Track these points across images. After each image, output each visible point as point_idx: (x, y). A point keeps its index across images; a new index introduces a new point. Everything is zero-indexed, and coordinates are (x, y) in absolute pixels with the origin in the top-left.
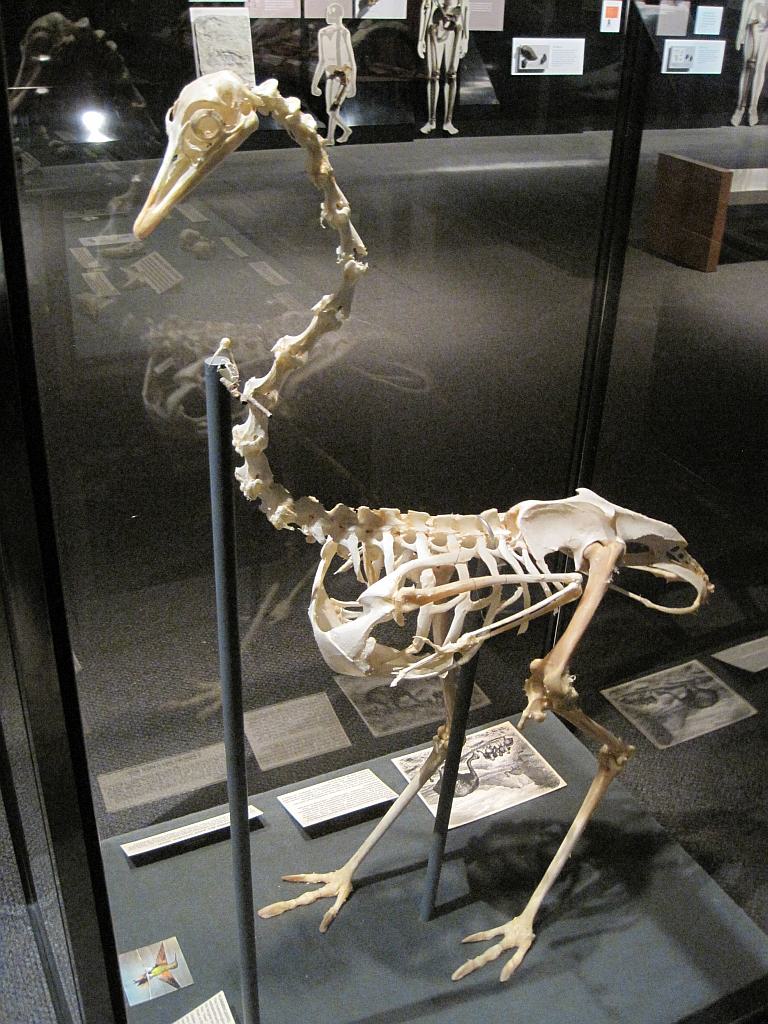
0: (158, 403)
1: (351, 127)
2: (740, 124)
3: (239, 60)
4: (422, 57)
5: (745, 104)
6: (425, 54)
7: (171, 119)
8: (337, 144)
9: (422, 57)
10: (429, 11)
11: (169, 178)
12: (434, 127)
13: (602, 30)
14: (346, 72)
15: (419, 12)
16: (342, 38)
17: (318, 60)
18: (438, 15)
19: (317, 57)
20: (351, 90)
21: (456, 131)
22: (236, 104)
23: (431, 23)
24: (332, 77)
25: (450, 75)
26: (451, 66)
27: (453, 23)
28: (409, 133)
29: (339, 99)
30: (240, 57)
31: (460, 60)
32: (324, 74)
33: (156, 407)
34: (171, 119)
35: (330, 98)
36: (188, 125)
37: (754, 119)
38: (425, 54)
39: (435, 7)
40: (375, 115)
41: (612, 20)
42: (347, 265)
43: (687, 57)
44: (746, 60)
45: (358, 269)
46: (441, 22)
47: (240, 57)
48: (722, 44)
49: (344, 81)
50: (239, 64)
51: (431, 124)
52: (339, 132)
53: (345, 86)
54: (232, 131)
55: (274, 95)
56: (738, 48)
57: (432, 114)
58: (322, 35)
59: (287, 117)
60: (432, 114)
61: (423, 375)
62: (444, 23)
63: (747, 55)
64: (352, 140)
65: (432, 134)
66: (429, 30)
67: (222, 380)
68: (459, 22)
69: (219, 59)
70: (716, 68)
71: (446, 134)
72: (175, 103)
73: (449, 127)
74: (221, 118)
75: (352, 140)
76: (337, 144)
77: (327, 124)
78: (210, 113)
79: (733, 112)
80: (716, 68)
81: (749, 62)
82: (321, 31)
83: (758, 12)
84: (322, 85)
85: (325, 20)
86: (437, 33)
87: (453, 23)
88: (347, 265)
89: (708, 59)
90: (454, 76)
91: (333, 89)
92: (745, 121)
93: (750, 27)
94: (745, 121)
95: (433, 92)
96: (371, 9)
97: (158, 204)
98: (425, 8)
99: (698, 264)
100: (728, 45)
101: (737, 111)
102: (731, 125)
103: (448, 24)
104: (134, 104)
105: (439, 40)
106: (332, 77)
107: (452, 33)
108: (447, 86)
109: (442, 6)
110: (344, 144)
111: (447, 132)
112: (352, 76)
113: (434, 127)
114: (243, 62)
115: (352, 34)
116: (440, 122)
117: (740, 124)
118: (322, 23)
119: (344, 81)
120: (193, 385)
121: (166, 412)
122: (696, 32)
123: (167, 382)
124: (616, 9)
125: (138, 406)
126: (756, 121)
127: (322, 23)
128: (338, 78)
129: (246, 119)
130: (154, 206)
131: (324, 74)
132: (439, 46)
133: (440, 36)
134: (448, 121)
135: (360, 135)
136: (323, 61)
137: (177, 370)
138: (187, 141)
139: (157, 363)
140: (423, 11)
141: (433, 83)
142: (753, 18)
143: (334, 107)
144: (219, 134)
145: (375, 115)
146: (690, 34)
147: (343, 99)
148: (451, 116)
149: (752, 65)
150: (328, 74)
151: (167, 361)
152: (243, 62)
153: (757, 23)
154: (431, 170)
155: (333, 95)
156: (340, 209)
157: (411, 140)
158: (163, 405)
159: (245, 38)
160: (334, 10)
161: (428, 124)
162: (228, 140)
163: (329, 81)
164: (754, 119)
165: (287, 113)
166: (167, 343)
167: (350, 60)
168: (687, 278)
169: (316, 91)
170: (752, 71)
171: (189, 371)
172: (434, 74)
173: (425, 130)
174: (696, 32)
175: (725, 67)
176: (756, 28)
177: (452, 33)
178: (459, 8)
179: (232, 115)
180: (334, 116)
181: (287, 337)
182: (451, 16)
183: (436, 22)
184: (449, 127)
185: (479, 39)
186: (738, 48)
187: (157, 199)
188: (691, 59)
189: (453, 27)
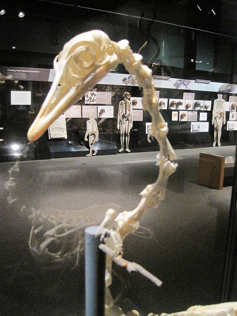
0: (36, 247)
1: (97, 150)
2: (215, 146)
3: (62, 130)
4: (119, 129)
5: (216, 140)
6: (120, 128)
7: (57, 61)
8: (93, 156)
9: (119, 129)
10: (120, 115)
11: (55, 99)
12: (123, 150)
13: (173, 120)
14: (95, 134)
15: (118, 115)
16: (94, 123)
17: (87, 130)
18: (124, 116)
19: (87, 129)
20: (97, 139)
21: (130, 151)
22: (104, 48)
23: (121, 119)
24: (91, 135)
25: (127, 134)
26: (128, 131)
27: (128, 119)
28: (115, 152)
29: (93, 141)
30: (62, 129)
31: (130, 129)
32: (89, 134)
33: (35, 249)
34: (57, 61)
35: (91, 141)
36: (71, 57)
37: (219, 144)
38: (120, 128)
39: (122, 114)
40: (104, 147)
41: (175, 117)
42: (165, 165)
43: (198, 127)
44: (215, 128)
45: (172, 167)
46: (124, 118)
47: (62, 129)
48: (208, 123)
49: (95, 136)
50: (62, 131)
51: (122, 149)
52: (93, 152)
53: (95, 137)
54: (102, 64)
55: (127, 48)
56: (213, 124)
57: (122, 146)
58: (88, 123)
59: (134, 64)
60: (122, 146)
61: (149, 230)
62: (125, 119)
63: (215, 127)
64: (97, 155)
65: (122, 152)
66: (120, 121)
67: (101, 246)
68: (130, 118)
69: (56, 130)
70: (207, 130)
71: (127, 152)
72: (60, 53)
73: (128, 150)
74: (95, 53)
75: (97, 155)
76: (93, 156)
77: (89, 149)
78: (87, 49)
79: (213, 143)
80: (207, 130)
81: (216, 128)
82: (87, 121)
83: (217, 114)
84: (88, 137)
85: (89, 118)
86: (123, 122)
87: (128, 119)
88: (165, 165)
89: (204, 128)
90: (129, 134)
91: (91, 138)
92: (217, 145)
93: (215, 118)
94: (217, 145)
95: (122, 139)
96: (103, 115)
97: (46, 116)
98: (119, 114)
99: (217, 188)
100: (209, 124)
101: (214, 142)
102: (213, 146)
103: (126, 119)
104: (30, 112)
105: (124, 124)
106: (91, 135)
107: (128, 121)
108: (127, 137)
109: (124, 114)
110: (95, 155)
111: (127, 151)
112: (97, 135)
113: (123, 150)
114: (63, 131)
115: (97, 123)
116: (125, 148)
117: (215, 146)
118: (88, 119)
119: (95, 136)
120: (52, 239)
121: (39, 251)
122: (200, 120)
123: (40, 237)
124: (176, 114)
125: (26, 249)
126: (220, 145)
127: (88, 119)
128: (93, 135)
129: (111, 58)
130: (43, 117)
131: (89, 134)
132: (124, 126)
133: (124, 122)
134: (127, 148)
135: (100, 153)
136: (88, 130)
137: (45, 232)
138: (70, 69)
139: (35, 229)
140: (118, 115)
141: (122, 136)
142: (216, 115)
143: (92, 144)
144: (93, 65)
145: (104, 147)
146: (198, 120)
147: (94, 142)
148: (128, 146)
149: (217, 129)
150: (90, 134)
151: (40, 228)
152: (63, 131)
153: (217, 117)
154: (124, 163)
155: (92, 140)
156: (163, 128)
157: (116, 154)
158: (38, 248)
159: (64, 123)
160: (91, 115)
161: (121, 149)
162: (98, 70)
163: (90, 136)
164: (219, 144)
165: (135, 61)
166: (41, 219)
167: (97, 130)
168: (213, 192)
169: (86, 139)
170: (217, 131)
171: (50, 232)
172: (122, 134)
173: (120, 151)
174: (200, 120)
175: (209, 130)
176: (217, 119)
177: (128, 121)
178: (129, 114)
179: (102, 54)
180: (92, 147)
181: (125, 212)
182: (127, 117)
183: (123, 118)
184: (128, 150)
185: (136, 124)
186: (213, 124)
187: (45, 114)
188: (199, 127)
189: (128, 120)
